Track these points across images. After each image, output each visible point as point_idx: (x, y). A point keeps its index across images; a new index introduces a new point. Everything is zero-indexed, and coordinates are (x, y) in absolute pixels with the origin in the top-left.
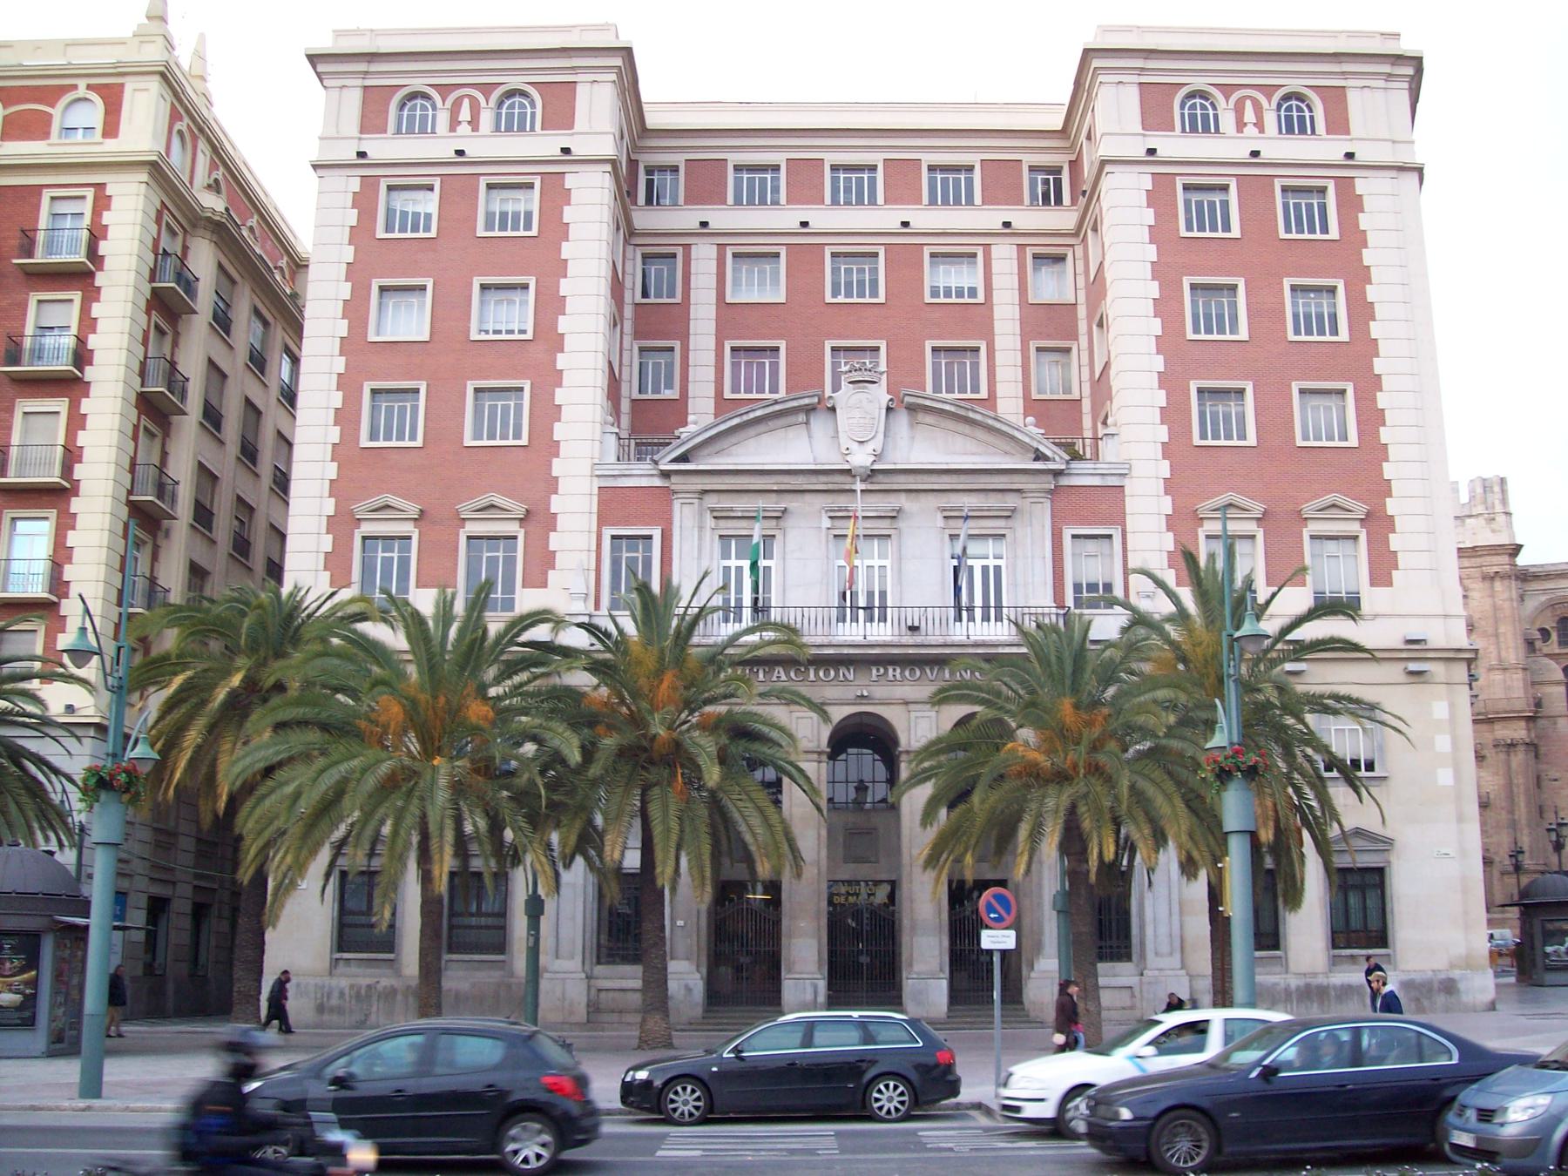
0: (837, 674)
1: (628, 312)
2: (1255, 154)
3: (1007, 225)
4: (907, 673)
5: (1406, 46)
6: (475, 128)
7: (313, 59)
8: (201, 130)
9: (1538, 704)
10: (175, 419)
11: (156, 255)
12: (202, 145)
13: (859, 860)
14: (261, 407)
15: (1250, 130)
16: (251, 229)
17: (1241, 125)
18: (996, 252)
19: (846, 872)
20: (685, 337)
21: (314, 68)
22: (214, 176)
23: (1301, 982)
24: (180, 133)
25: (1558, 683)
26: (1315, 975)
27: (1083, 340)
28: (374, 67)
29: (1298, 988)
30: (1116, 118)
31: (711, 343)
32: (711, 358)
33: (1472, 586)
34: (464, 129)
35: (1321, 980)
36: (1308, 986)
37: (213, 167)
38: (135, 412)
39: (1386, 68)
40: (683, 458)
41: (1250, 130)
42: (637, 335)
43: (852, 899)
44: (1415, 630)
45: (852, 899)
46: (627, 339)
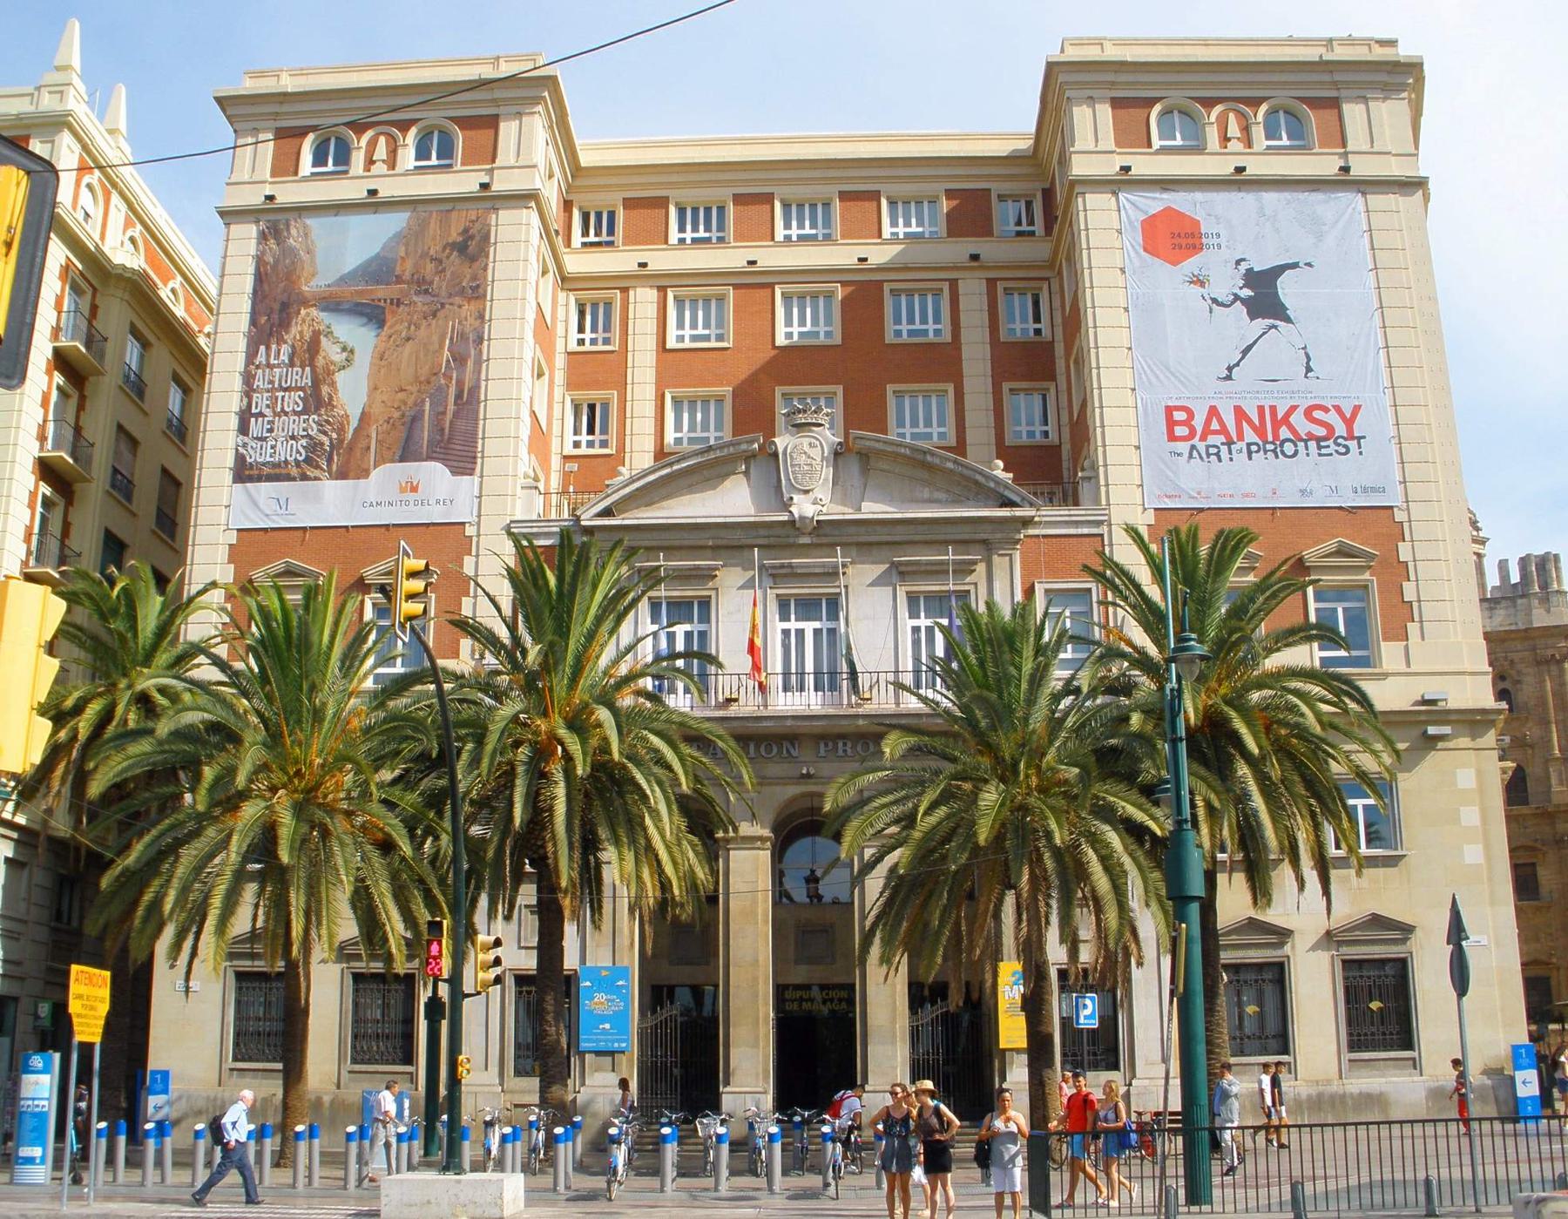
0: (780, 752)
1: (560, 361)
2: (1240, 170)
3: (975, 257)
4: (859, 748)
5: (1404, 51)
6: (392, 165)
7: (219, 100)
8: (114, 185)
9: (1120, 1139)
10: (77, 487)
11: (59, 313)
12: (115, 198)
13: (812, 961)
14: (182, 479)
15: (1235, 146)
16: (173, 291)
17: (1225, 139)
18: (962, 287)
19: (799, 975)
20: (622, 386)
21: (224, 110)
22: (129, 233)
23: (1313, 1091)
24: (89, 186)
25: (814, 843)
26: (1329, 1082)
27: (1061, 379)
28: (286, 108)
29: (1310, 1097)
30: (1093, 140)
31: (650, 392)
32: (650, 409)
33: (1525, 671)
34: (379, 168)
35: (1335, 1087)
36: (1320, 1095)
37: (128, 224)
38: (33, 478)
39: (1384, 77)
40: (607, 512)
41: (1235, 146)
42: (570, 385)
43: (806, 1006)
44: (1430, 688)
45: (806, 1006)
46: (558, 392)
